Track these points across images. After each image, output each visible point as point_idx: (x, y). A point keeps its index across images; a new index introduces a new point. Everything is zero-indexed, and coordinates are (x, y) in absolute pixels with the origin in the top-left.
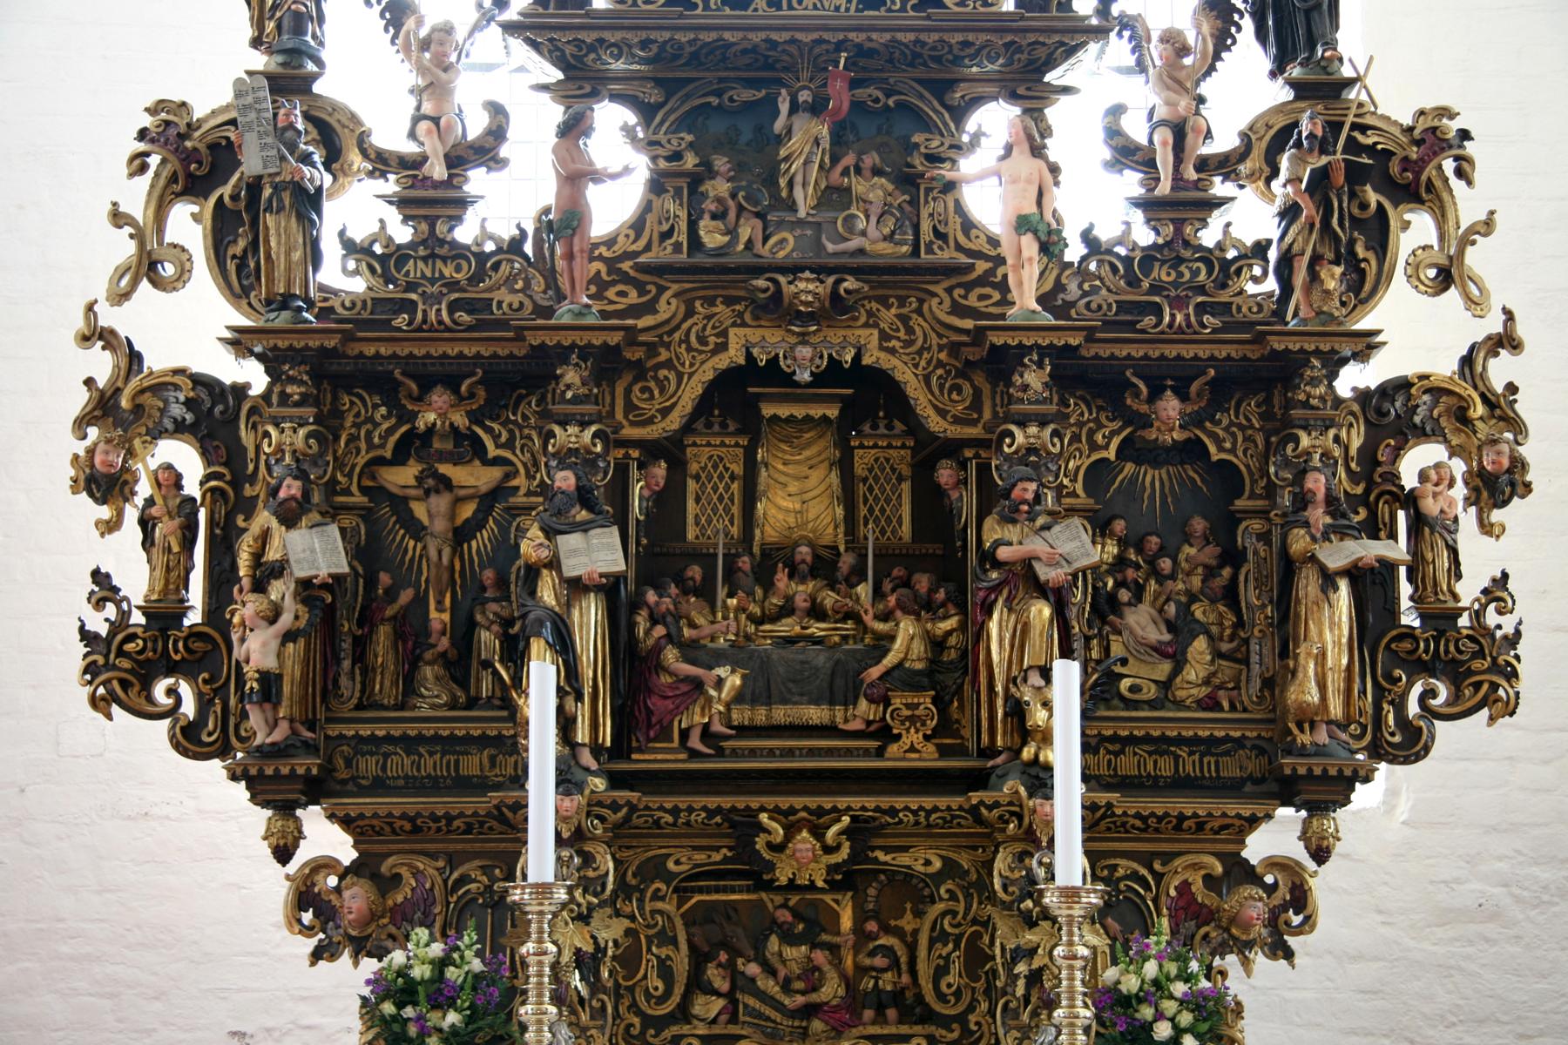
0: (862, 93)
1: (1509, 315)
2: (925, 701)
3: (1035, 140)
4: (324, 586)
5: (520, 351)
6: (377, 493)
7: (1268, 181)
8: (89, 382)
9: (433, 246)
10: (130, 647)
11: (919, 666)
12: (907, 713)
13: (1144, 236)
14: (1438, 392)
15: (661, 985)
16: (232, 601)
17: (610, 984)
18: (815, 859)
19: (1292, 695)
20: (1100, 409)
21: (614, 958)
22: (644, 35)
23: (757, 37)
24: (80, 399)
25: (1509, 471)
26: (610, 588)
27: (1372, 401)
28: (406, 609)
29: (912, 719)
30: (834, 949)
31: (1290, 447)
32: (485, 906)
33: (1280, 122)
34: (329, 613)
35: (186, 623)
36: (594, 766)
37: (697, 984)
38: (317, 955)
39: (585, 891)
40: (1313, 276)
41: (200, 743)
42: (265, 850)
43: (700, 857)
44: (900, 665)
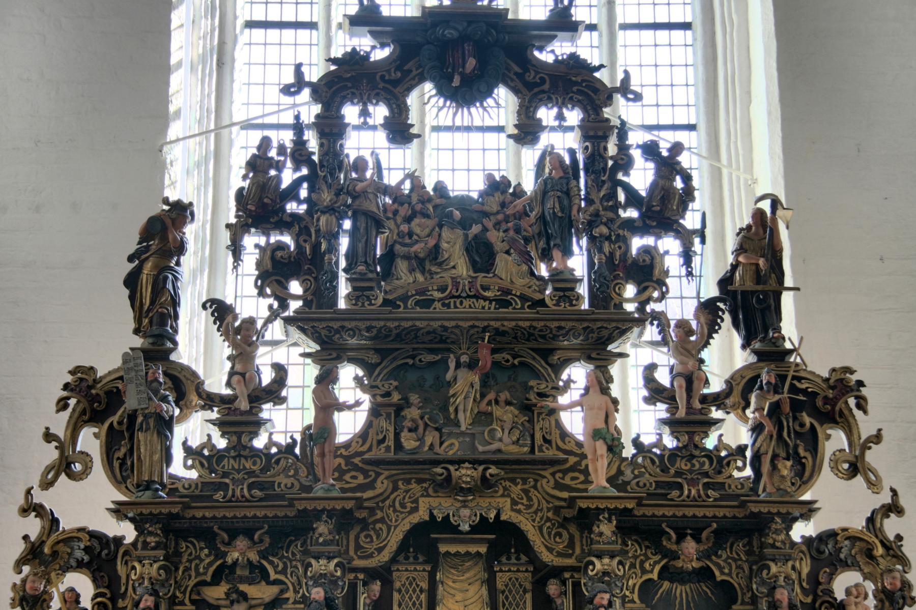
0: (499, 357)
1: (894, 492)
5: (291, 513)
7: (744, 409)
13: (670, 442)
14: (854, 539)
22: (368, 323)
23: (436, 324)
31: (765, 572)
33: (750, 375)
40: (774, 467)
44: (102, 424)
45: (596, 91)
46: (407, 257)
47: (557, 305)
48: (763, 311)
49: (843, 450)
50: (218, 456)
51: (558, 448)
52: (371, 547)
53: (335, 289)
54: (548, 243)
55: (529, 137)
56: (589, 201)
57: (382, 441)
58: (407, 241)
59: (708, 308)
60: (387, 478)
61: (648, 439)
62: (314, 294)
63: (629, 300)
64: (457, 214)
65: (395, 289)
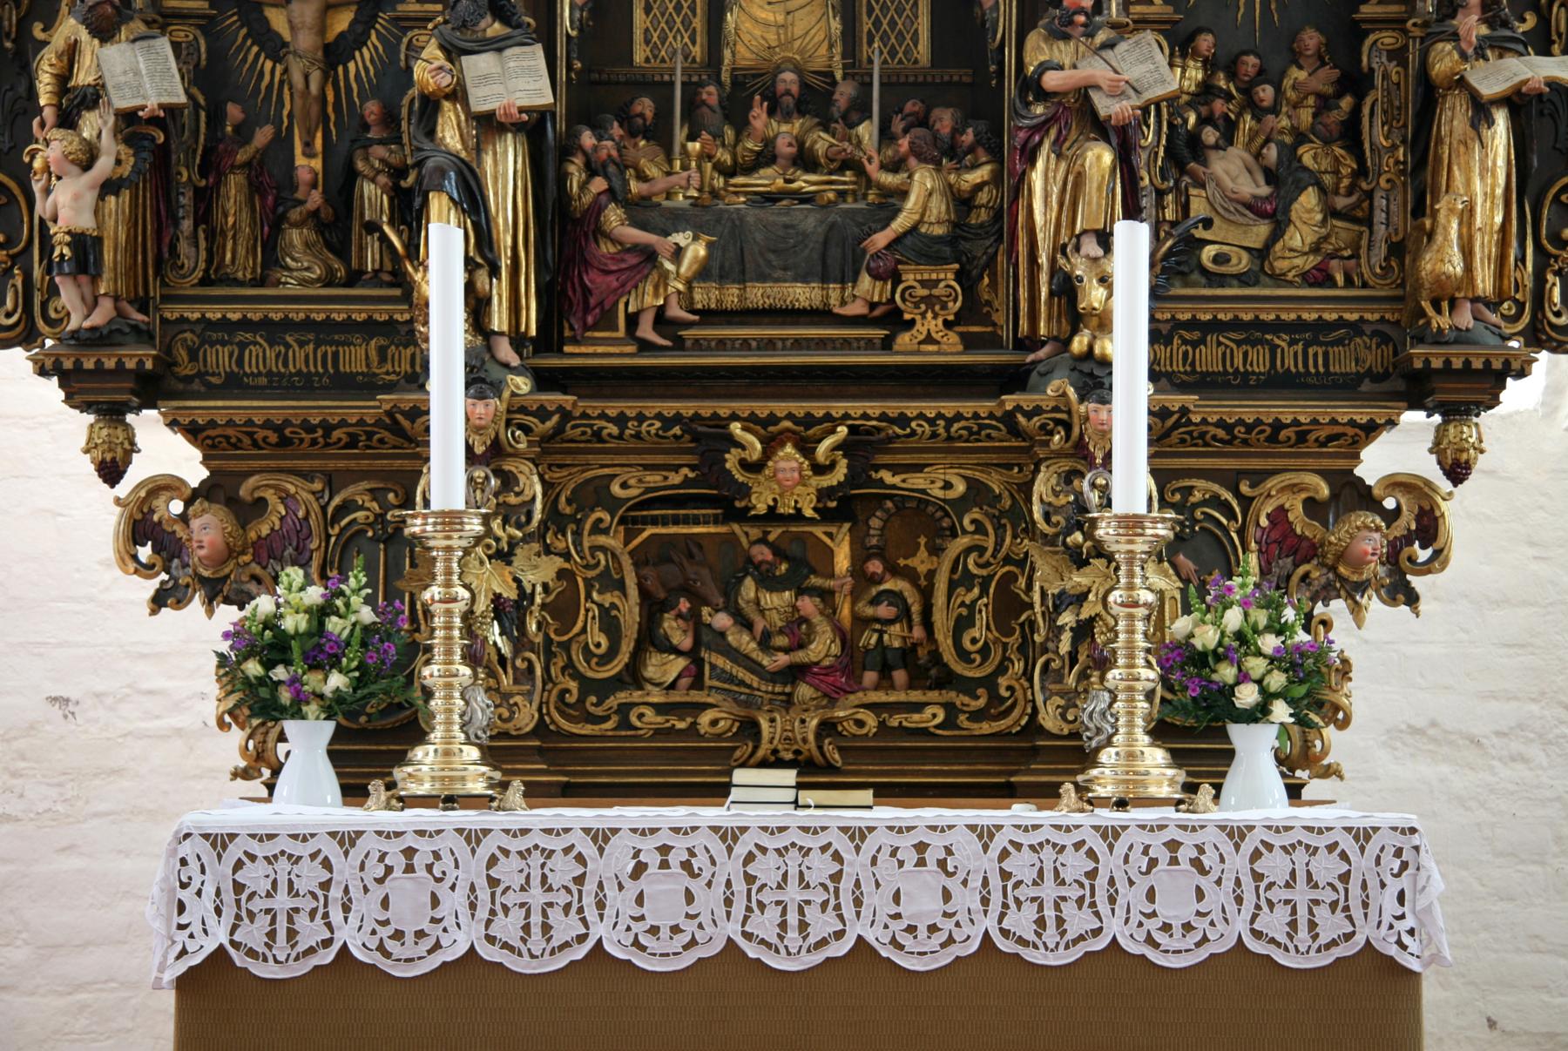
2: (947, 276)
4: (153, 121)
11: (939, 231)
12: (922, 292)
17: (539, 639)
18: (803, 481)
21: (543, 606)
26: (532, 127)
28: (265, 151)
29: (929, 301)
30: (826, 595)
32: (375, 540)
36: (515, 361)
37: (650, 639)
38: (159, 601)
39: (505, 522)
42: (87, 467)
43: (654, 479)
44: (913, 230)
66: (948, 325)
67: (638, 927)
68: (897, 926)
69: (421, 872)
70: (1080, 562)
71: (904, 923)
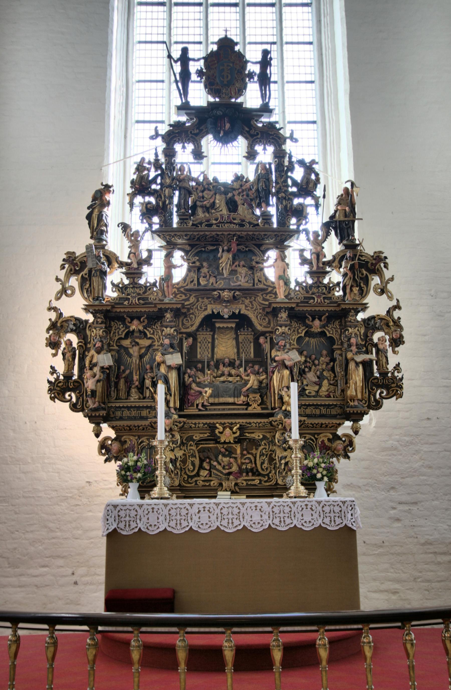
0: (240, 247)
1: (398, 301)
2: (258, 396)
3: (282, 258)
4: (107, 368)
5: (156, 310)
6: (120, 346)
7: (339, 268)
8: (50, 320)
9: (134, 284)
10: (60, 385)
11: (256, 387)
12: (253, 399)
13: (310, 281)
14: (382, 319)
15: (192, 467)
16: (84, 373)
17: (179, 467)
18: (231, 435)
19: (349, 393)
20: (300, 324)
21: (180, 461)
22: (186, 233)
23: (214, 233)
24: (48, 324)
25: (399, 338)
26: (178, 368)
27: (366, 322)
28: (128, 375)
29: (254, 401)
30: (235, 458)
31: (347, 332)
32: (148, 448)
33: (342, 254)
34: (108, 375)
35: (73, 378)
36: (175, 412)
37: (201, 467)
38: (106, 461)
39: (173, 444)
40: (351, 290)
41: (77, 408)
42: (93, 435)
43: (202, 435)
44: (251, 387)
45: (279, 138)
46: (202, 207)
47: (264, 225)
48: (347, 229)
49: (378, 284)
50: (125, 287)
51: (264, 284)
52: (188, 324)
53: (172, 219)
54: (260, 200)
55: (252, 157)
56: (277, 183)
57: (192, 281)
58: (202, 200)
59: (327, 226)
60: (195, 297)
61: (301, 280)
62: (164, 222)
63: (293, 225)
64: (222, 189)
65: (197, 220)
66: (258, 405)
67: (199, 524)
68: (252, 523)
69: (155, 512)
70: (285, 450)
71: (253, 522)
